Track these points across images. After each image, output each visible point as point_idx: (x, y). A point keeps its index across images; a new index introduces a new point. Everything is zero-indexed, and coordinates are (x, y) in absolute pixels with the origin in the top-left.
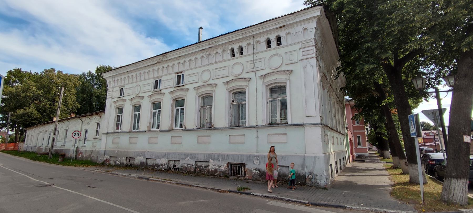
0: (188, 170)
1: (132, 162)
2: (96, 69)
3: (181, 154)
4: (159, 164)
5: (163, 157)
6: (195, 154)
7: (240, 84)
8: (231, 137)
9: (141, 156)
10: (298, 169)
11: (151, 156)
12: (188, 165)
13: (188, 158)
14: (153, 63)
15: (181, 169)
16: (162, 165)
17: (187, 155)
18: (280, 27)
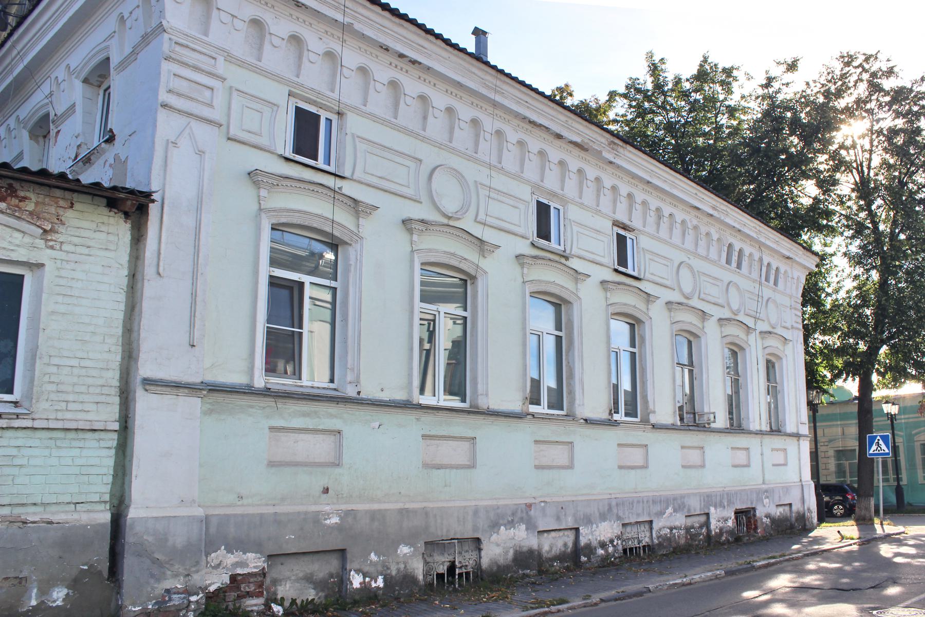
0: (674, 545)
1: (465, 560)
2: (681, 67)
3: (654, 502)
4: (595, 543)
5: (603, 517)
6: (683, 497)
7: (773, 359)
8: (745, 463)
9: (511, 524)
10: (112, 214)
11: (558, 519)
12: (671, 529)
13: (670, 510)
14: (565, 133)
15: (660, 544)
16: (603, 545)
17: (666, 501)
18: (532, 123)
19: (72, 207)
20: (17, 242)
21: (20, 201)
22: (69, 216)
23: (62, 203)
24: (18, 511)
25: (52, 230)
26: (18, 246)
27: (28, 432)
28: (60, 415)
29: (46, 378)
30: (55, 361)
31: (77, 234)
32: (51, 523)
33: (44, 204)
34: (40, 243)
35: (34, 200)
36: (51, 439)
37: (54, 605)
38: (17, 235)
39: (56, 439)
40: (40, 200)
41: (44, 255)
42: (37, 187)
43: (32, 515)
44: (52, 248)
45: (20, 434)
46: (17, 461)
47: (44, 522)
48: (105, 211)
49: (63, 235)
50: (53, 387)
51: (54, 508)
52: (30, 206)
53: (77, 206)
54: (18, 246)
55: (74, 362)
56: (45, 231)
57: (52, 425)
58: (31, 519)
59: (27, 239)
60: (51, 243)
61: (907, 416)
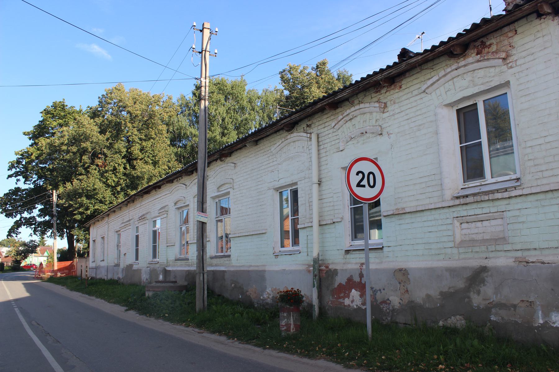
19: (516, 33)
20: (492, 74)
21: (489, 48)
22: (517, 40)
23: (510, 34)
24: (526, 254)
25: (508, 56)
26: (493, 76)
27: (523, 198)
28: (539, 182)
29: (526, 158)
30: (529, 144)
31: (524, 49)
32: (543, 263)
33: (501, 42)
34: (504, 68)
35: (495, 43)
36: (537, 200)
37: (555, 326)
38: (492, 70)
39: (540, 200)
40: (498, 41)
41: (508, 75)
42: (494, 33)
43: (532, 257)
44: (511, 67)
45: (519, 200)
46: (521, 219)
47: (539, 262)
48: (537, 21)
49: (517, 54)
50: (531, 163)
51: (546, 252)
52: (494, 48)
53: (519, 31)
54: (493, 76)
55: (541, 141)
56: (504, 59)
57: (534, 191)
58: (531, 260)
59: (498, 69)
60: (510, 65)
61: (207, 84)
